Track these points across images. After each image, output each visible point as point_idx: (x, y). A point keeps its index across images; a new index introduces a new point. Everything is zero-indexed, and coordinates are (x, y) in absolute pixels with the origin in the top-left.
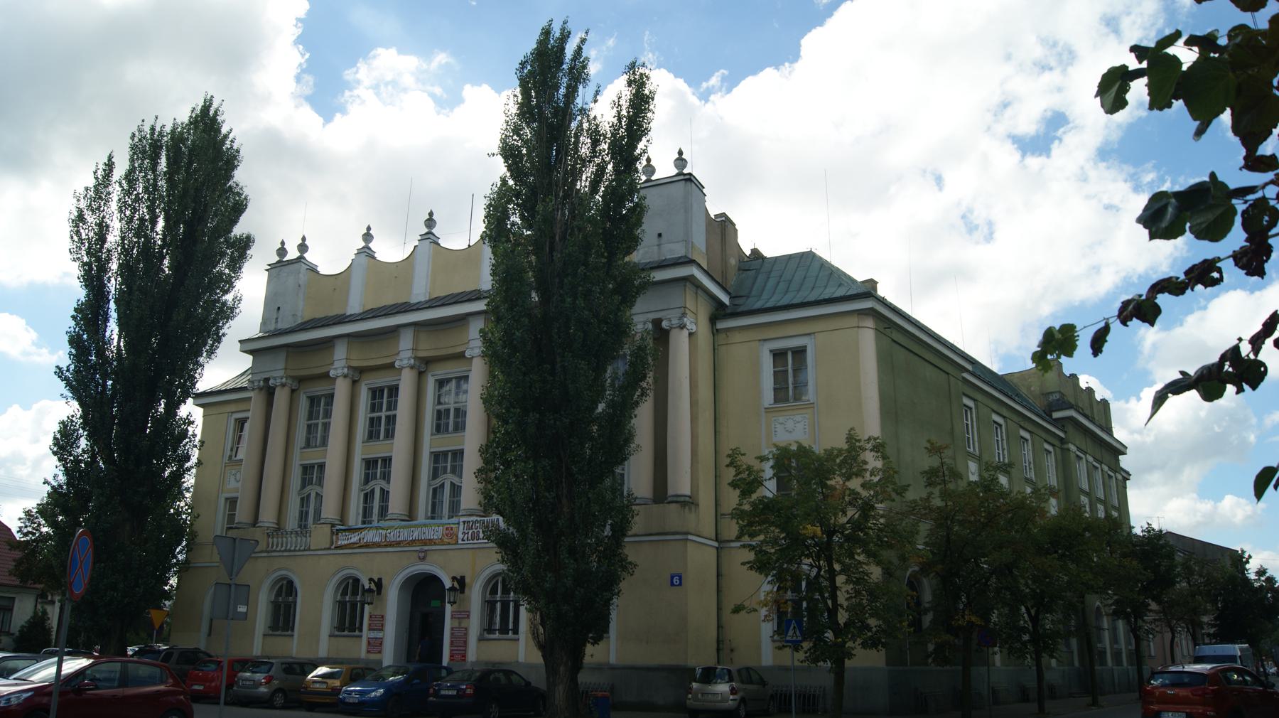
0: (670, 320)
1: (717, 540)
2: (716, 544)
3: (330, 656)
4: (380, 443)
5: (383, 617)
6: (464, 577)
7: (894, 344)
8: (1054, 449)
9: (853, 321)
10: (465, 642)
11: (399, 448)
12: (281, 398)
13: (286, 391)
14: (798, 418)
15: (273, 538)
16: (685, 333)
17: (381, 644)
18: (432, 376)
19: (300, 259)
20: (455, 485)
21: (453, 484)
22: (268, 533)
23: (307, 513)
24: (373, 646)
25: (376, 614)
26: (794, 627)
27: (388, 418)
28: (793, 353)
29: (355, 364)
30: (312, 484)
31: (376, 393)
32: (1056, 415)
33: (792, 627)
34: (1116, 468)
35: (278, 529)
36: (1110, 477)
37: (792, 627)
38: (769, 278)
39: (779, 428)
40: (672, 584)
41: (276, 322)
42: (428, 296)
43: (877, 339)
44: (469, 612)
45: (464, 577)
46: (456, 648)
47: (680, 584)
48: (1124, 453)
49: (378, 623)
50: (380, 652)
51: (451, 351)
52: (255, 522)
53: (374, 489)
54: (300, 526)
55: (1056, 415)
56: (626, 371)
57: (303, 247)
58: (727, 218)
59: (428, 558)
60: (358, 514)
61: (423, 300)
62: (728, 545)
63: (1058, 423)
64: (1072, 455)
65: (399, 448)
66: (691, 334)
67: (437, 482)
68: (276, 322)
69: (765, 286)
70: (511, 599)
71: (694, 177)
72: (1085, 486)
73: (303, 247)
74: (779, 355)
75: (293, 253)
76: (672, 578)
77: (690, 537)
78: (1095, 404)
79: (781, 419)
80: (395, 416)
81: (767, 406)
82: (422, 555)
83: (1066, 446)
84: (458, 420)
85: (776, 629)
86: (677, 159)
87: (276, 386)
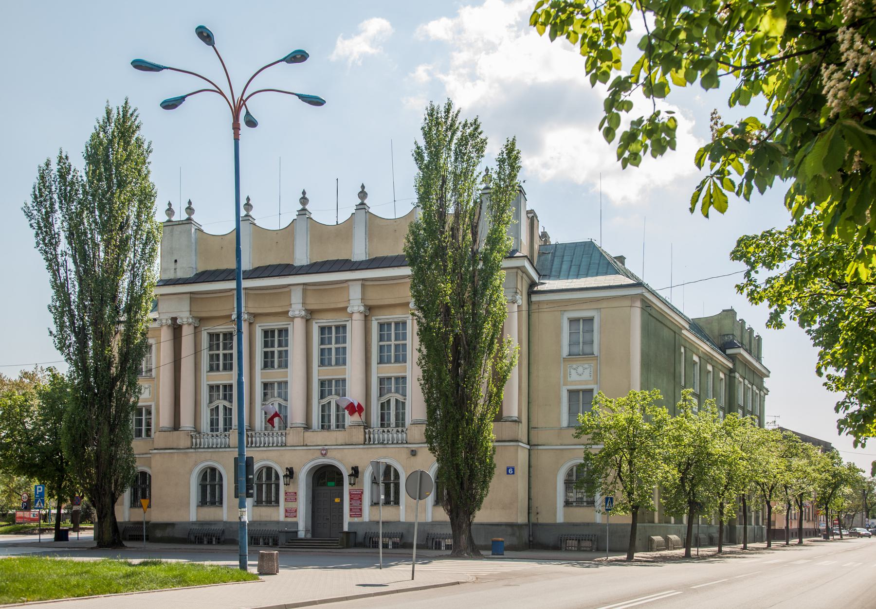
0: (182, 319)
1: (529, 444)
2: (528, 447)
3: (255, 519)
4: (274, 371)
5: (295, 493)
7: (650, 317)
8: (700, 360)
9: (627, 303)
10: (361, 510)
11: (295, 374)
12: (187, 333)
13: (191, 329)
14: (586, 366)
15: (196, 439)
16: (516, 305)
17: (296, 511)
19: (189, 220)
27: (280, 352)
28: (583, 320)
29: (252, 311)
31: (267, 333)
32: (729, 352)
34: (761, 388)
35: (197, 430)
36: (757, 394)
38: (562, 261)
39: (573, 372)
40: (508, 473)
41: (175, 272)
43: (642, 314)
47: (513, 473)
48: (768, 376)
49: (292, 497)
50: (295, 517)
51: (333, 306)
52: (176, 426)
54: (212, 430)
55: (729, 352)
56: (865, 478)
57: (190, 210)
58: (535, 214)
59: (328, 454)
60: (262, 422)
61: (305, 264)
62: (536, 447)
63: (732, 358)
64: (736, 381)
65: (295, 374)
66: (518, 306)
67: (325, 401)
68: (175, 272)
69: (561, 268)
71: (653, 293)
72: (741, 403)
73: (190, 210)
74: (573, 321)
75: (180, 215)
76: (508, 469)
77: (521, 444)
78: (744, 331)
79: (574, 366)
80: (286, 351)
81: (565, 356)
82: (324, 452)
83: (733, 375)
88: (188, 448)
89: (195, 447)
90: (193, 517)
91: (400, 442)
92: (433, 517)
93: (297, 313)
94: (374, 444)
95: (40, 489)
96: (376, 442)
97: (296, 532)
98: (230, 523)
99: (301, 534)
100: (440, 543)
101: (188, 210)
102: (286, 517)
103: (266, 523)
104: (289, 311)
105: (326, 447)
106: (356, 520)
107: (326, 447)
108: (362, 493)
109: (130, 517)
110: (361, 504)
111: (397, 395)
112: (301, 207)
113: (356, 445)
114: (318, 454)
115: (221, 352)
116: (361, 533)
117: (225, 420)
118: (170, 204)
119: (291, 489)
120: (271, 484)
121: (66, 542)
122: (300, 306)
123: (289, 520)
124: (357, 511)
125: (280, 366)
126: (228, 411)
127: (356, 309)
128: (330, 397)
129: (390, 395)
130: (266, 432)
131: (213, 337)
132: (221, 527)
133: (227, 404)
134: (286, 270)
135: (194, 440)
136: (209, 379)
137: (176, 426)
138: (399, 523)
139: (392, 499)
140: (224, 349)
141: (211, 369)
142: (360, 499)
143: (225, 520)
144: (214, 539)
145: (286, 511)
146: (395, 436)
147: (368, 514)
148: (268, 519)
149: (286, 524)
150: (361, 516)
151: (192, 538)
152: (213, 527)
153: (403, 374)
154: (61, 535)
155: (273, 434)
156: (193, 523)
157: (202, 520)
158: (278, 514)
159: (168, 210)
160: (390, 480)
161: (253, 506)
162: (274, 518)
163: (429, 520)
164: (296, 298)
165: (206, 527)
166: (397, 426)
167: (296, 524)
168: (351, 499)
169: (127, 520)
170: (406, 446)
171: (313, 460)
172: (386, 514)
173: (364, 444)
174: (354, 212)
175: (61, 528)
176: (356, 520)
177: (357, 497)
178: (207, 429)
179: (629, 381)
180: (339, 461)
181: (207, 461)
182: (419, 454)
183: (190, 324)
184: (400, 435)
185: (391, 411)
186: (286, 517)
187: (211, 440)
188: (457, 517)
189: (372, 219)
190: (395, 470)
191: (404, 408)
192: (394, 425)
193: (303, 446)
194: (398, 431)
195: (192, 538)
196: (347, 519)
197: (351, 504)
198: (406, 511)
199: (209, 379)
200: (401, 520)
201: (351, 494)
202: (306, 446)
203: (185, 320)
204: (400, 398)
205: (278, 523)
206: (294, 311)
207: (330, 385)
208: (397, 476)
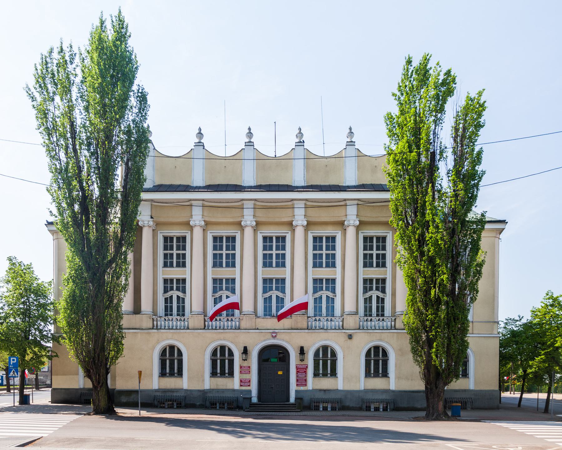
0: (143, 221)
5: (249, 367)
6: (246, 347)
10: (306, 380)
17: (250, 381)
18: (260, 233)
20: (379, 297)
21: (178, 297)
22: (153, 318)
23: (171, 307)
24: (244, 382)
25: (244, 366)
26: (14, 372)
30: (322, 290)
33: (13, 371)
37: (13, 371)
42: (255, 183)
44: (307, 365)
45: (246, 347)
46: (300, 383)
49: (245, 370)
50: (249, 386)
51: (277, 220)
53: (221, 296)
54: (166, 315)
59: (278, 337)
60: (312, 312)
70: (227, 358)
82: (274, 335)
84: (270, 260)
85: (160, 372)
86: (248, 133)
87: (144, 226)
88: (150, 329)
89: (155, 327)
90: (155, 386)
91: (182, 328)
92: (364, 386)
93: (248, 223)
94: (208, 329)
95: (13, 360)
96: (167, 328)
97: (251, 398)
98: (190, 390)
99: (255, 400)
100: (370, 407)
101: (249, 134)
102: (241, 386)
103: (223, 391)
104: (241, 221)
105: (277, 331)
106: (302, 388)
107: (277, 331)
108: (307, 367)
109: (84, 385)
110: (306, 376)
111: (327, 292)
112: (197, 141)
113: (301, 329)
114: (269, 336)
115: (375, 252)
116: (306, 399)
117: (178, 307)
118: (250, 129)
119: (245, 364)
120: (319, 360)
121: (27, 406)
122: (251, 218)
123: (244, 388)
124: (302, 381)
125: (378, 266)
126: (380, 301)
127: (300, 223)
128: (271, 292)
129: (322, 292)
130: (366, 318)
131: (168, 240)
132: (183, 394)
133: (381, 295)
134: (186, 188)
135: (155, 323)
136: (164, 273)
137: (137, 310)
138: (337, 391)
139: (176, 371)
140: (178, 249)
141: (165, 265)
142: (305, 372)
143: (471, 389)
144: (175, 404)
145: (241, 381)
146: (226, 323)
147: (312, 383)
148: (224, 388)
149: (242, 392)
150: (306, 385)
151: (208, 404)
152: (175, 394)
153: (232, 277)
154: (24, 400)
155: (184, 320)
156: (156, 391)
157: (163, 387)
158: (235, 383)
159: (198, 133)
160: (328, 357)
161: (210, 377)
162: (230, 387)
163: (362, 388)
164: (352, 211)
165: (168, 394)
166: (327, 315)
167: (250, 391)
168: (298, 372)
169: (82, 387)
170: (344, 331)
171: (265, 340)
172: (326, 383)
173: (204, 329)
174: (193, 148)
175: (25, 393)
176: (302, 388)
177: (302, 371)
178: (162, 314)
179: (494, 290)
180: (287, 342)
181: (168, 339)
182: (354, 337)
183: (150, 227)
184: (182, 323)
185: (323, 305)
186: (241, 386)
187: (226, 323)
188: (436, 388)
189: (360, 155)
190: (230, 350)
191: (184, 302)
192: (325, 315)
193: (255, 329)
194: (228, 320)
195: (156, 403)
196: (293, 387)
197: (297, 376)
198: (343, 382)
199: (164, 273)
200: (339, 389)
201: (297, 368)
202: (258, 329)
203: (146, 222)
204: (381, 295)
205: (234, 390)
206: (246, 221)
207: (221, 283)
208: (231, 353)
